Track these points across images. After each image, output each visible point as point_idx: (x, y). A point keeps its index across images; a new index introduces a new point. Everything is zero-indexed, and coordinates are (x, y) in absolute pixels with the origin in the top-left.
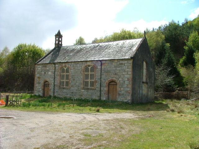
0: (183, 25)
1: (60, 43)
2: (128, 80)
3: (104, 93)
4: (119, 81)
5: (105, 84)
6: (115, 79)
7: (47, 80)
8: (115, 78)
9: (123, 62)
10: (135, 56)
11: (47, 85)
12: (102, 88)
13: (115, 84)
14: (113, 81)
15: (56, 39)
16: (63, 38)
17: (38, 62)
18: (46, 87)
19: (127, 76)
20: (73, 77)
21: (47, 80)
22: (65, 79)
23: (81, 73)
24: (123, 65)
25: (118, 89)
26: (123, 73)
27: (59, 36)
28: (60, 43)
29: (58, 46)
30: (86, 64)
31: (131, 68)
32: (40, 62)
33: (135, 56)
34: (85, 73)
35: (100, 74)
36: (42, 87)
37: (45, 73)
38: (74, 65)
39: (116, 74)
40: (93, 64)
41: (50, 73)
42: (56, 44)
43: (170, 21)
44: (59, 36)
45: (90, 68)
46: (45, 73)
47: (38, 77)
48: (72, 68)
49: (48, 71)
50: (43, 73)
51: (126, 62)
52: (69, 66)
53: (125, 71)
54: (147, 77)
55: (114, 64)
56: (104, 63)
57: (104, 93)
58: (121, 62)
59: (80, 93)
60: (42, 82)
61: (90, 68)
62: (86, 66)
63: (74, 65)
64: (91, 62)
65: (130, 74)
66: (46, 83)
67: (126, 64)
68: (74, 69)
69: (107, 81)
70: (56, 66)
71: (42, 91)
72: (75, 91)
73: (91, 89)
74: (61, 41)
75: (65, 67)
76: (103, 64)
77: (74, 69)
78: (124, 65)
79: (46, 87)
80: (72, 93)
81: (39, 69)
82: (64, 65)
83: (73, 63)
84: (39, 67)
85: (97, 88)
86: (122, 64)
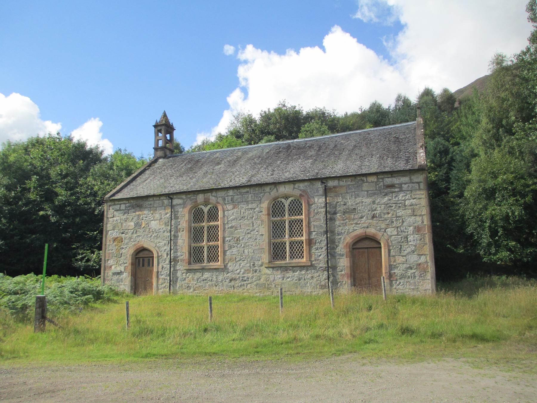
0: (95, 118)
2: (418, 230)
4: (387, 235)
9: (396, 180)
11: (141, 259)
13: (374, 245)
14: (366, 238)
15: (156, 135)
16: (175, 132)
17: (114, 195)
18: (143, 265)
21: (146, 246)
24: (397, 190)
26: (400, 212)
27: (165, 127)
30: (274, 193)
31: (423, 196)
32: (125, 190)
34: (193, 225)
38: (236, 197)
39: (373, 217)
40: (297, 193)
43: (373, 101)
45: (287, 203)
47: (115, 240)
51: (405, 179)
54: (88, 276)
56: (334, 187)
58: (388, 181)
60: (128, 251)
61: (287, 203)
62: (275, 199)
63: (236, 197)
64: (292, 186)
65: (418, 183)
66: (141, 255)
67: (405, 187)
73: (294, 268)
75: (206, 205)
76: (331, 189)
78: (401, 188)
79: (143, 265)
82: (200, 198)
83: (231, 192)
84: (117, 207)
86: (392, 186)
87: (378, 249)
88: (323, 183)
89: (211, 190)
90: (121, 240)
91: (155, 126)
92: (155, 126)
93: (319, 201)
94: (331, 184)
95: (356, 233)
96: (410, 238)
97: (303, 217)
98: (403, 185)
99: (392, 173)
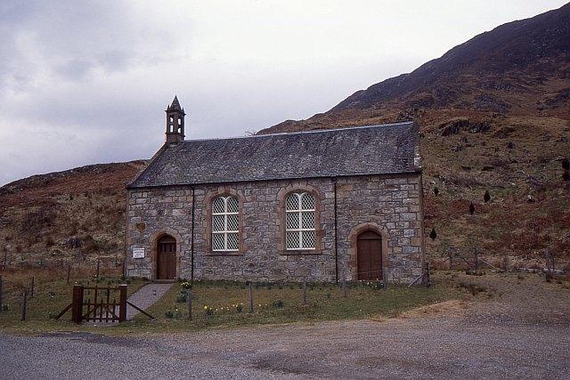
1: (179, 131)
2: (412, 225)
3: (349, 263)
4: (387, 229)
5: (348, 238)
6: (375, 224)
7: (169, 231)
8: (376, 221)
9: (395, 182)
10: (142, 169)
12: (340, 250)
15: (168, 120)
19: (406, 216)
20: (251, 223)
22: (300, 208)
23: (275, 211)
25: (386, 251)
27: (175, 112)
28: (179, 131)
29: (175, 137)
33: (73, 208)
35: (333, 214)
36: (154, 253)
37: (160, 213)
39: (376, 212)
41: (176, 212)
42: (168, 133)
44: (175, 112)
46: (160, 213)
47: (138, 225)
48: (248, 198)
49: (172, 206)
50: (154, 212)
52: (240, 192)
53: (401, 205)
55: (369, 185)
56: (343, 185)
57: (349, 263)
58: (389, 181)
59: (274, 264)
60: (152, 237)
65: (416, 212)
68: (254, 199)
69: (354, 232)
70: (196, 193)
71: (154, 263)
72: (260, 260)
74: (182, 126)
77: (254, 199)
80: (251, 265)
81: (140, 200)
84: (140, 195)
85: (325, 249)
86: (392, 186)
87: (375, 242)
88: (333, 181)
89: (231, 184)
90: (144, 227)
91: (167, 111)
92: (167, 111)
93: (329, 195)
94: (340, 182)
95: (361, 226)
96: (406, 231)
97: (226, 250)
98: (330, 278)
99: (392, 176)
